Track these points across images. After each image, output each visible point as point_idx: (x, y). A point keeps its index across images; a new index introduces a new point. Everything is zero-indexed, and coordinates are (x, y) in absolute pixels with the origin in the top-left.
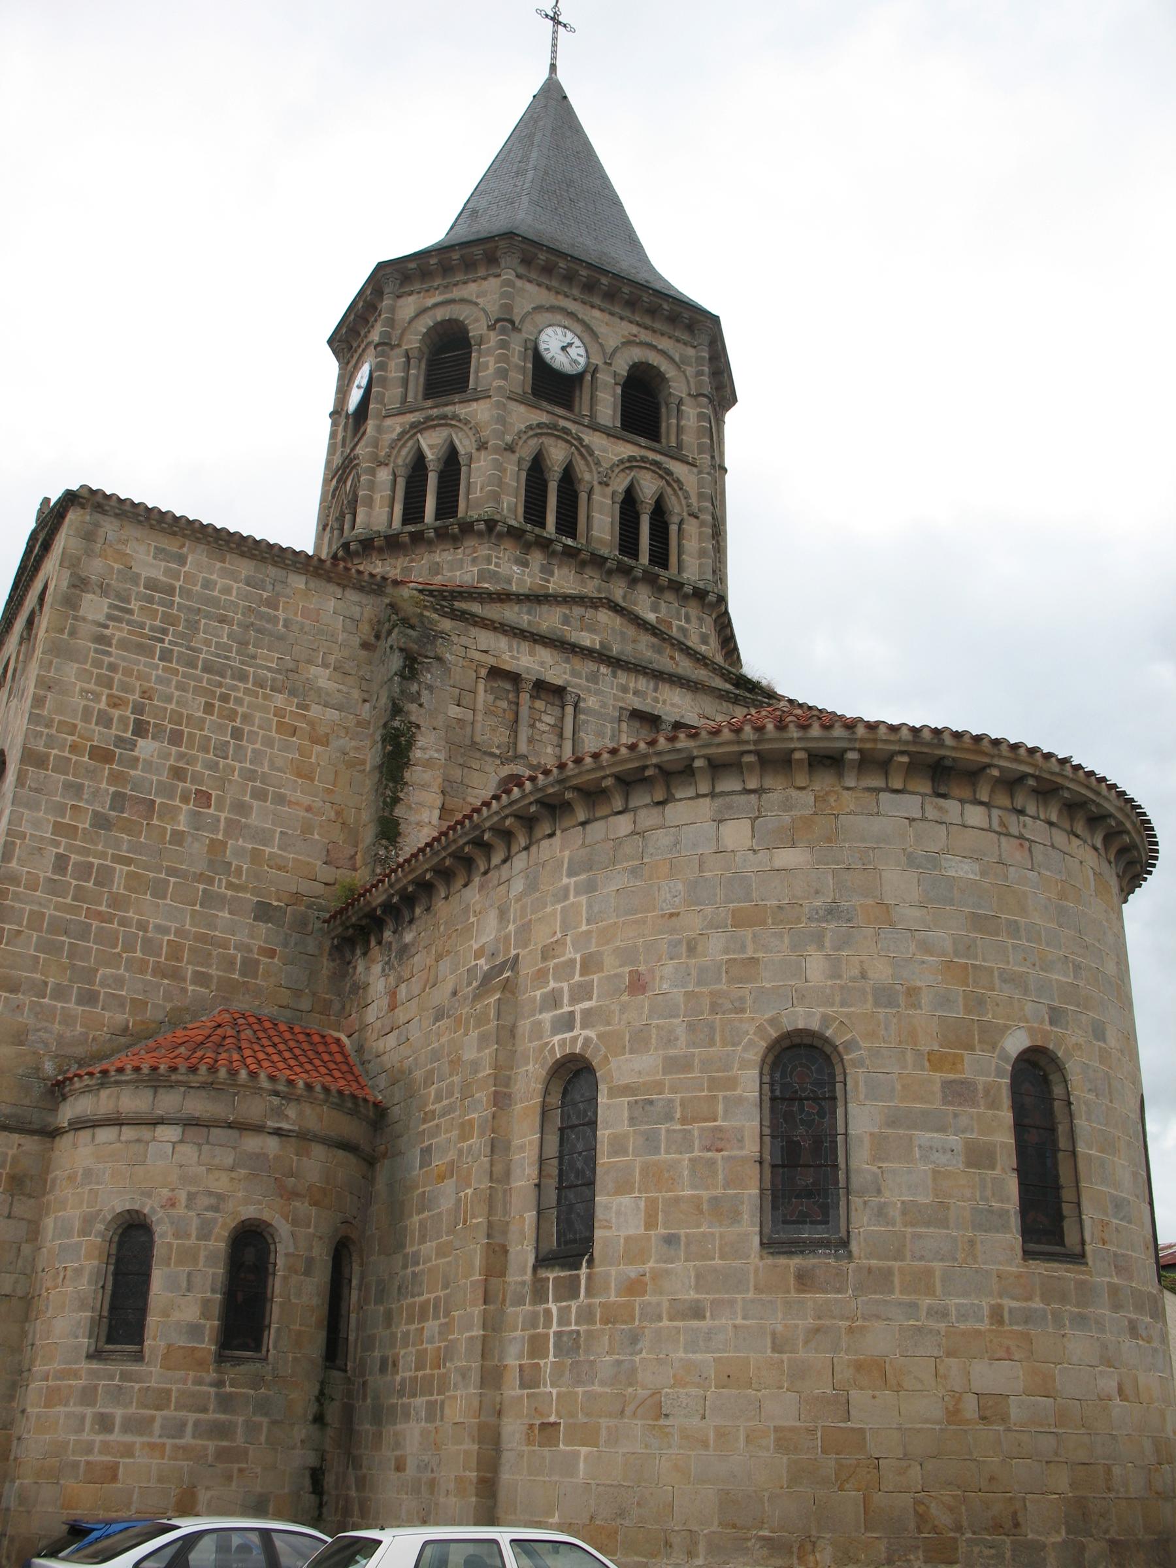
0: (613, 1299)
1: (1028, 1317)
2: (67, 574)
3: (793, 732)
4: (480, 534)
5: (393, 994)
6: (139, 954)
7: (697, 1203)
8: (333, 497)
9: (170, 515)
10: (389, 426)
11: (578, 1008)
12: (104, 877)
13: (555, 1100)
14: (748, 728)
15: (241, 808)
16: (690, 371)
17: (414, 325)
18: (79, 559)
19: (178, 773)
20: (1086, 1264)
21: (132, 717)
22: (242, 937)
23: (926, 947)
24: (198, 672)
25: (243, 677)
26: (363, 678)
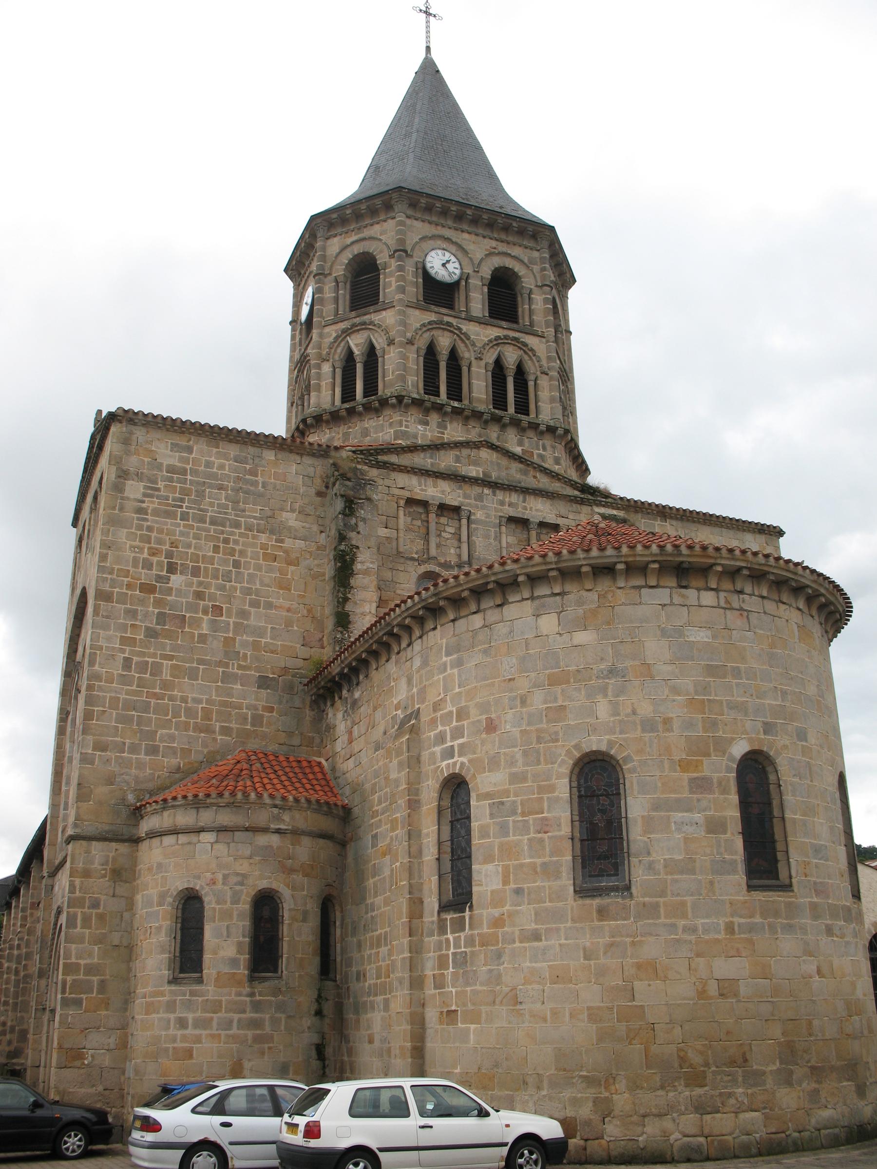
0: (485, 930)
1: (751, 928)
2: (114, 469)
3: (581, 554)
4: (393, 406)
5: (350, 733)
6: (183, 719)
7: (533, 866)
8: (296, 382)
9: (179, 421)
10: (328, 333)
11: (456, 743)
12: (156, 670)
13: (446, 803)
14: (550, 554)
15: (244, 614)
16: (536, 268)
17: (339, 258)
18: (121, 458)
19: (199, 595)
20: (793, 891)
21: (166, 560)
22: (251, 700)
23: (675, 690)
24: (207, 525)
25: (237, 525)
26: (319, 517)
